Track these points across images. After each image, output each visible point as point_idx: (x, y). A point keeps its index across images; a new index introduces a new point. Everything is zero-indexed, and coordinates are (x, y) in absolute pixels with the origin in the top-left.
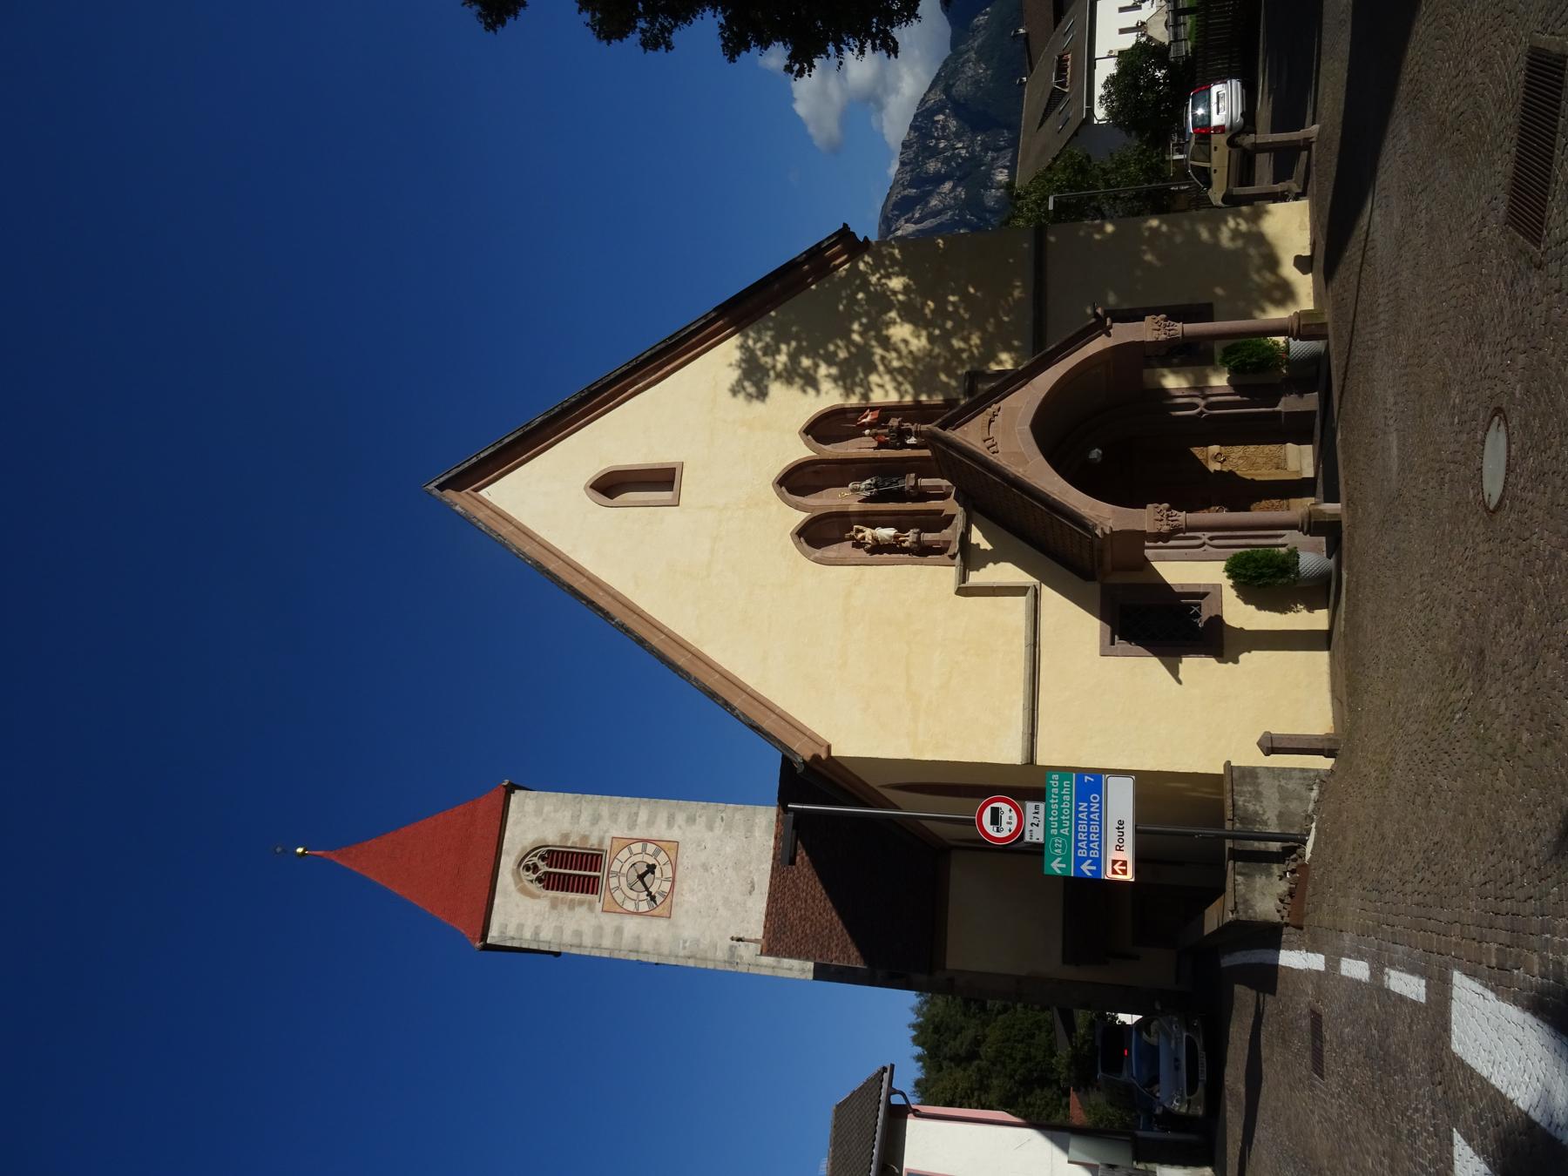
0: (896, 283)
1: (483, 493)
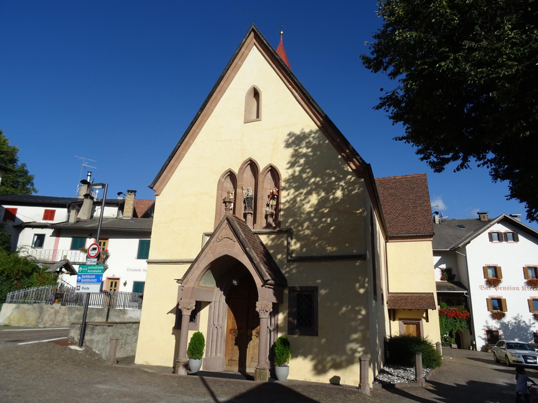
0: (339, 194)
1: (254, 47)
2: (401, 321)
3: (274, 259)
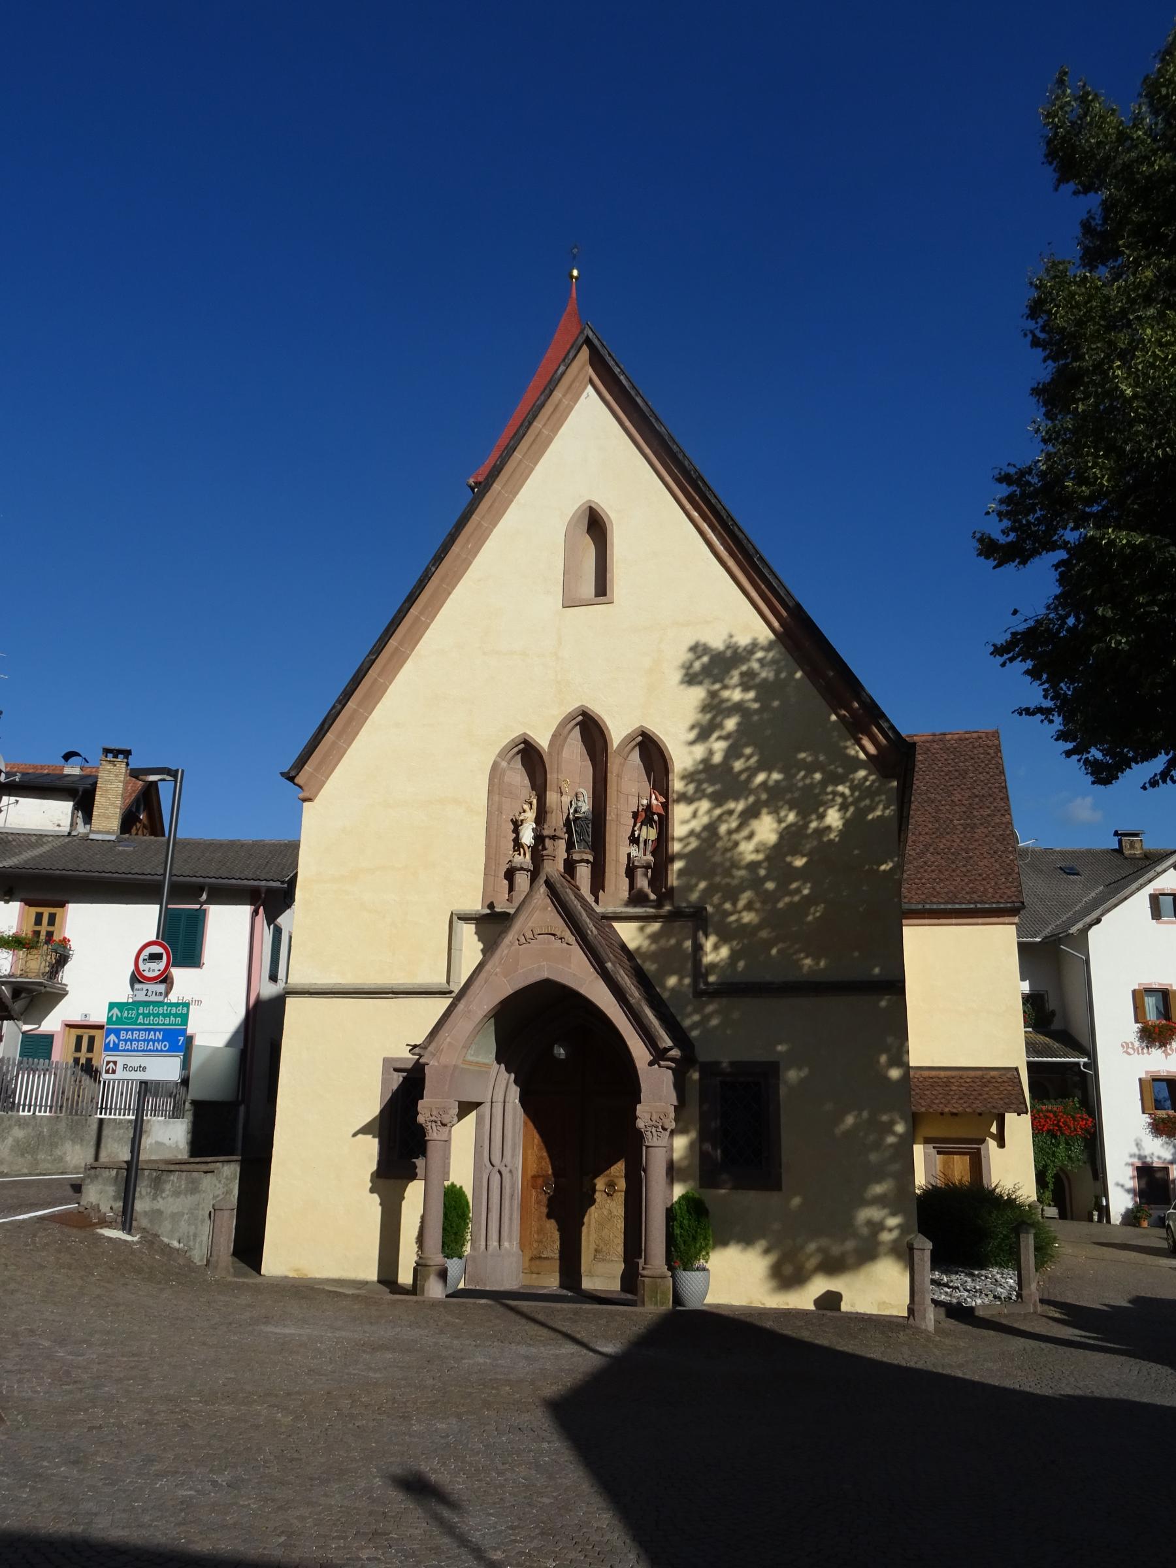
0: (834, 818)
1: (590, 389)
2: (931, 1146)
3: (658, 990)
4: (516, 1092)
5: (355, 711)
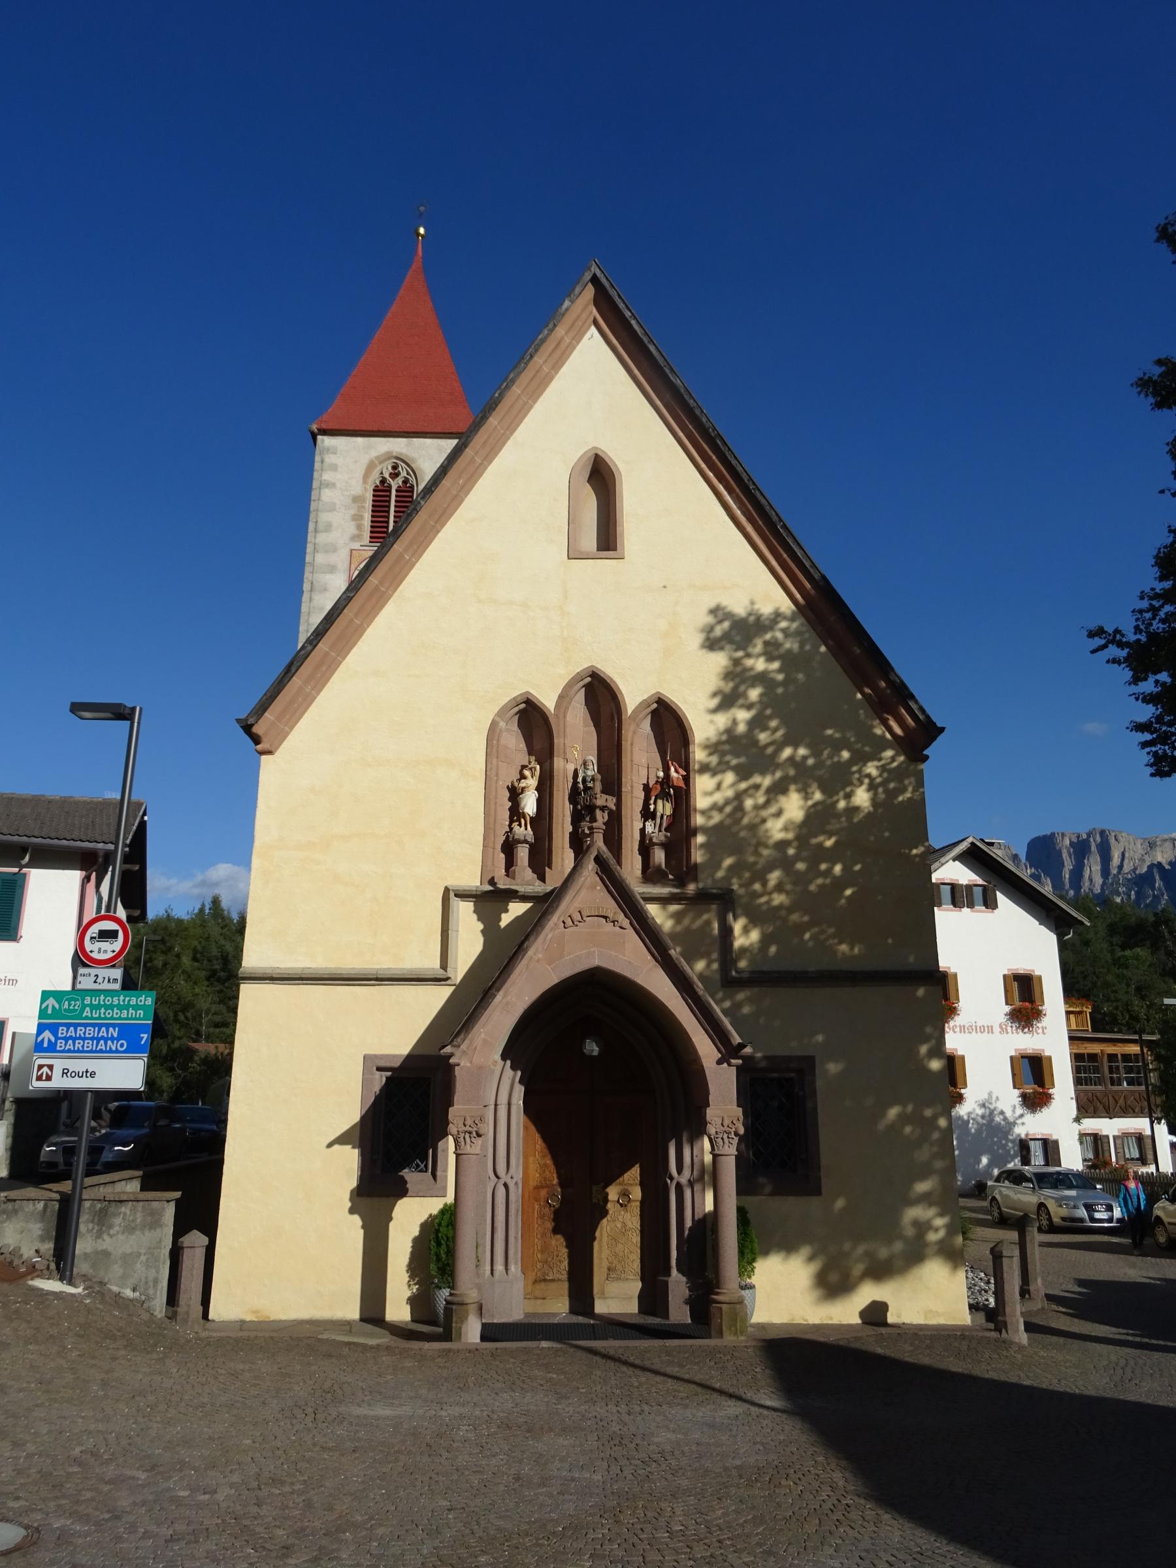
0: (862, 797)
1: (593, 329)
4: (520, 1091)
5: (326, 654)
